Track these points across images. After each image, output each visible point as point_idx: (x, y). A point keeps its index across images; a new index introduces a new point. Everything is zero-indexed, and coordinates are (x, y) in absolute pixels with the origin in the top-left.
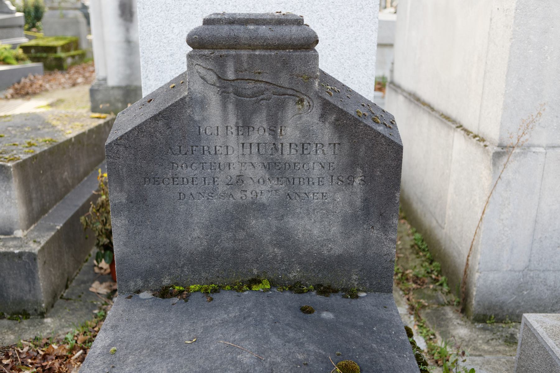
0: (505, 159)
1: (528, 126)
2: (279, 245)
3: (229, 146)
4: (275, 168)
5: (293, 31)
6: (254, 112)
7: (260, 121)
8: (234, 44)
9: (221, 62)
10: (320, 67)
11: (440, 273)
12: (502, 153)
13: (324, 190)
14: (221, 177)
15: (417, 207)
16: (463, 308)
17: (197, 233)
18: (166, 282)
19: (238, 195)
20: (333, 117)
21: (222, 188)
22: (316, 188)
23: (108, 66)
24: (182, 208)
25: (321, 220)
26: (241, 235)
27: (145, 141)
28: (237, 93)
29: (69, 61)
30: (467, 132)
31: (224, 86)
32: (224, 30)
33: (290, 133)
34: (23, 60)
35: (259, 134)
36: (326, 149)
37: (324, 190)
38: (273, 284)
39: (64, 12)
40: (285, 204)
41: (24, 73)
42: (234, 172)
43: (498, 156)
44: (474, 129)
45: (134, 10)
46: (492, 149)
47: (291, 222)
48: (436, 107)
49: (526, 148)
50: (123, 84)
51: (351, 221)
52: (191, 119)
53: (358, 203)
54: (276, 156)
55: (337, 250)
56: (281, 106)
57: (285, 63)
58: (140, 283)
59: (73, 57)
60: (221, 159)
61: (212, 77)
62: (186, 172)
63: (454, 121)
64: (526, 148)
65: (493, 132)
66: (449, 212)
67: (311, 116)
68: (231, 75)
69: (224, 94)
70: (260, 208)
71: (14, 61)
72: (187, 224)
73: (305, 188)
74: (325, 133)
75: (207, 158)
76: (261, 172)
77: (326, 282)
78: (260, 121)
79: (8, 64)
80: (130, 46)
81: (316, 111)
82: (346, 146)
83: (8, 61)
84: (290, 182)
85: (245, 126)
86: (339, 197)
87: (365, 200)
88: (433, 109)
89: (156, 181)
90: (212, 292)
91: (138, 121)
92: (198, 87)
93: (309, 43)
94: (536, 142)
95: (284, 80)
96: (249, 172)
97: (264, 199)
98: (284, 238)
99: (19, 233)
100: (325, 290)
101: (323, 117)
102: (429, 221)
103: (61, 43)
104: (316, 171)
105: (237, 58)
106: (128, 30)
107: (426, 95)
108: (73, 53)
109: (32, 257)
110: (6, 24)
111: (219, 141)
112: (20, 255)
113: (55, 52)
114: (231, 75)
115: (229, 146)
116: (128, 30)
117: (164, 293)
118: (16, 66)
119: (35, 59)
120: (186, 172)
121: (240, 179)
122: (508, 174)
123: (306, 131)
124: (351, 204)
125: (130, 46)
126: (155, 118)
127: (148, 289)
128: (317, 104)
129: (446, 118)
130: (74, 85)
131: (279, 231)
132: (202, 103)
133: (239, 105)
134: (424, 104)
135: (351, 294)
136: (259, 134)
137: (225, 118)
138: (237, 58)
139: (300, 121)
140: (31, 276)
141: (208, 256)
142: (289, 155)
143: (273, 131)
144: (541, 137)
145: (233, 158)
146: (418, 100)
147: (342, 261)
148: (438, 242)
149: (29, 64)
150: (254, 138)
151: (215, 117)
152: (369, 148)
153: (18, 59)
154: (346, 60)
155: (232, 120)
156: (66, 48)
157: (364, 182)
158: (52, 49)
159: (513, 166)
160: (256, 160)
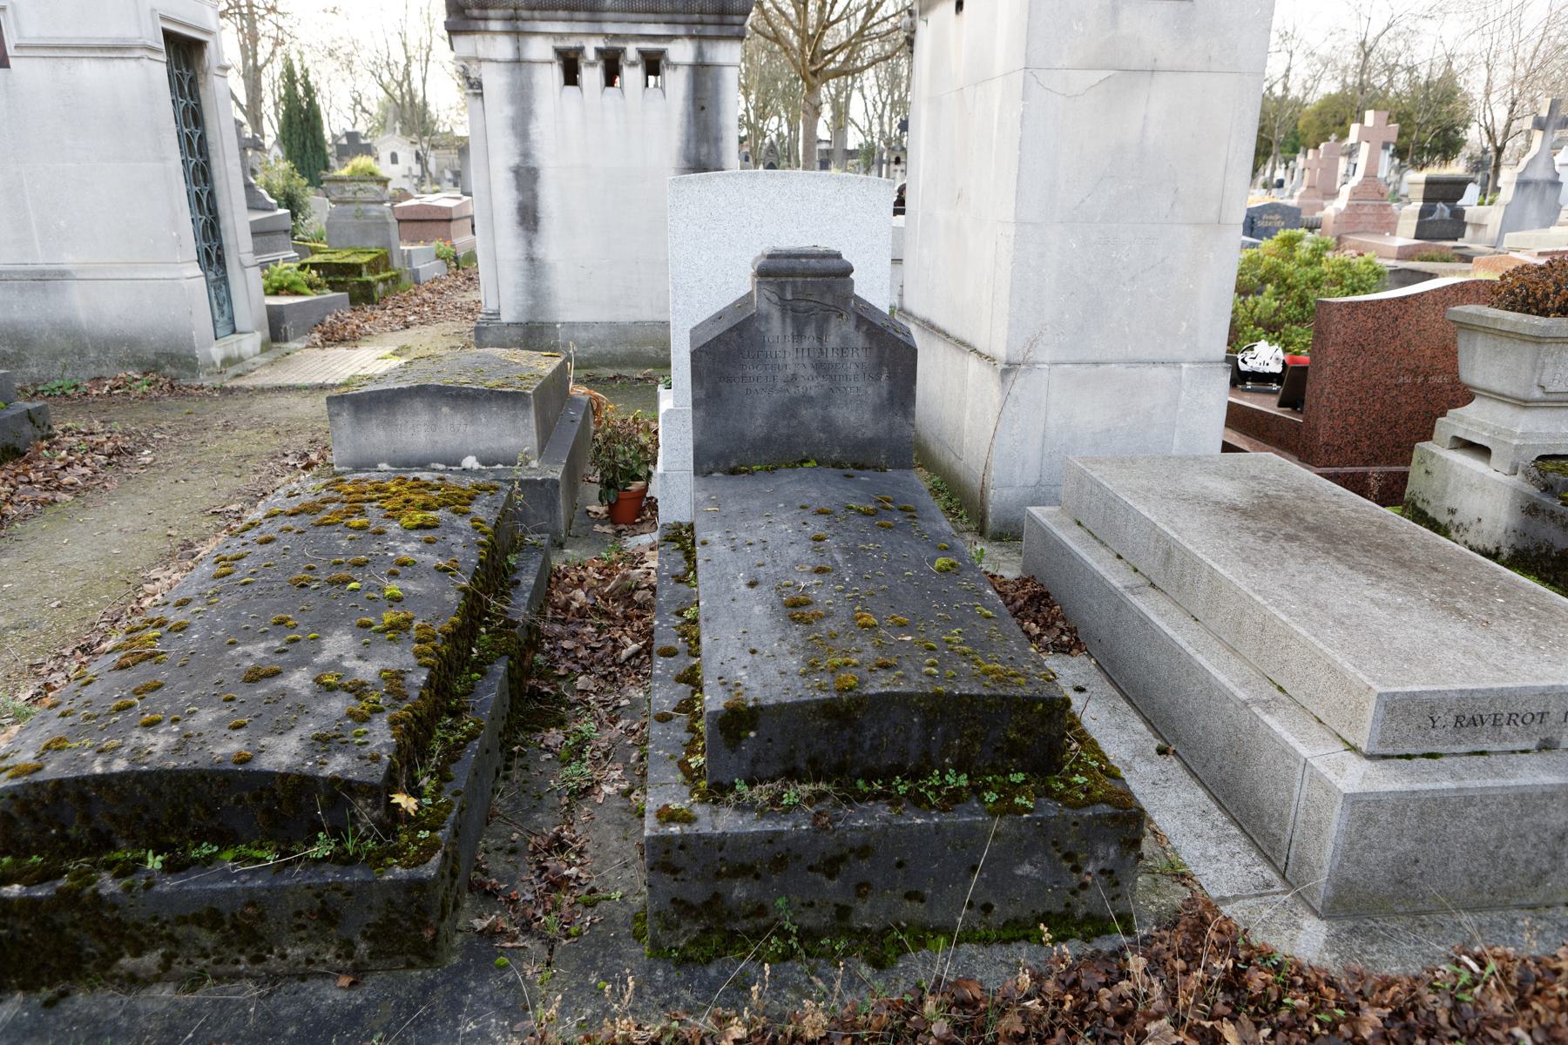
0: (1012, 376)
1: (1032, 344)
2: (823, 430)
3: (787, 352)
4: (821, 367)
5: (833, 263)
6: (806, 324)
7: (810, 331)
8: (792, 273)
9: (782, 287)
10: (857, 291)
11: (960, 507)
12: (1009, 370)
13: (859, 385)
14: (780, 375)
15: (935, 448)
16: (981, 532)
17: (759, 422)
18: (733, 464)
19: (792, 390)
20: (864, 328)
21: (780, 385)
22: (852, 383)
23: (500, 291)
24: (749, 401)
25: (855, 412)
26: (794, 423)
27: (722, 348)
28: (793, 310)
29: (381, 286)
30: (980, 354)
31: (783, 305)
32: (784, 263)
33: (833, 340)
34: (319, 286)
35: (809, 342)
36: (859, 354)
37: (859, 385)
38: (819, 463)
39: (362, 207)
40: (828, 396)
41: (327, 306)
42: (790, 371)
43: (1005, 372)
44: (985, 351)
45: (541, 215)
46: (1000, 366)
47: (833, 411)
48: (951, 333)
49: (1031, 365)
50: (523, 320)
51: (880, 410)
52: (758, 330)
53: (885, 393)
54: (823, 358)
55: (869, 434)
56: (826, 320)
57: (829, 287)
58: (712, 466)
59: (384, 281)
60: (780, 362)
61: (775, 298)
62: (752, 372)
63: (968, 346)
64: (1031, 365)
65: (1001, 351)
66: (966, 440)
67: (849, 327)
68: (789, 296)
69: (783, 311)
70: (808, 400)
71: (308, 291)
72: (752, 415)
73: (844, 383)
74: (859, 340)
75: (770, 361)
76: (810, 371)
77: (860, 461)
78: (810, 331)
79: (297, 293)
80: (533, 265)
81: (852, 323)
82: (875, 349)
83: (299, 288)
84: (832, 379)
85: (799, 335)
86: (870, 390)
87: (890, 392)
88: (948, 336)
89: (729, 380)
90: (771, 469)
91: (716, 333)
92: (764, 306)
93: (848, 270)
94: (1040, 359)
95: (828, 300)
96: (801, 372)
97: (812, 393)
98: (827, 424)
99: (534, 464)
100: (862, 467)
101: (857, 327)
102: (947, 458)
103: (367, 258)
104: (853, 370)
105: (794, 284)
106: (530, 243)
107: (941, 322)
108: (383, 275)
109: (554, 483)
110: (268, 228)
111: (779, 347)
112: (543, 482)
113: (360, 275)
114: (789, 296)
115: (787, 352)
116: (530, 243)
117: (733, 472)
118: (313, 297)
119: (333, 286)
120: (752, 372)
121: (795, 377)
122: (1016, 390)
123: (844, 338)
124: (879, 395)
125: (533, 265)
126: (730, 330)
127: (718, 471)
128: (853, 317)
129: (961, 344)
130: (407, 326)
131: (823, 419)
132: (767, 318)
133: (794, 319)
134: (939, 331)
135: (877, 468)
136: (809, 342)
137: (784, 330)
138: (794, 284)
139: (840, 331)
140: (552, 505)
141: (767, 440)
142: (832, 357)
143: (820, 339)
144: (1044, 354)
145: (789, 360)
146: (933, 327)
147: (871, 444)
148: (957, 477)
149: (330, 294)
150: (806, 344)
151: (777, 329)
152: (891, 352)
153: (311, 286)
154: (872, 286)
155: (789, 331)
156: (374, 267)
157: (889, 377)
158: (354, 269)
159: (1020, 381)
160: (806, 361)
